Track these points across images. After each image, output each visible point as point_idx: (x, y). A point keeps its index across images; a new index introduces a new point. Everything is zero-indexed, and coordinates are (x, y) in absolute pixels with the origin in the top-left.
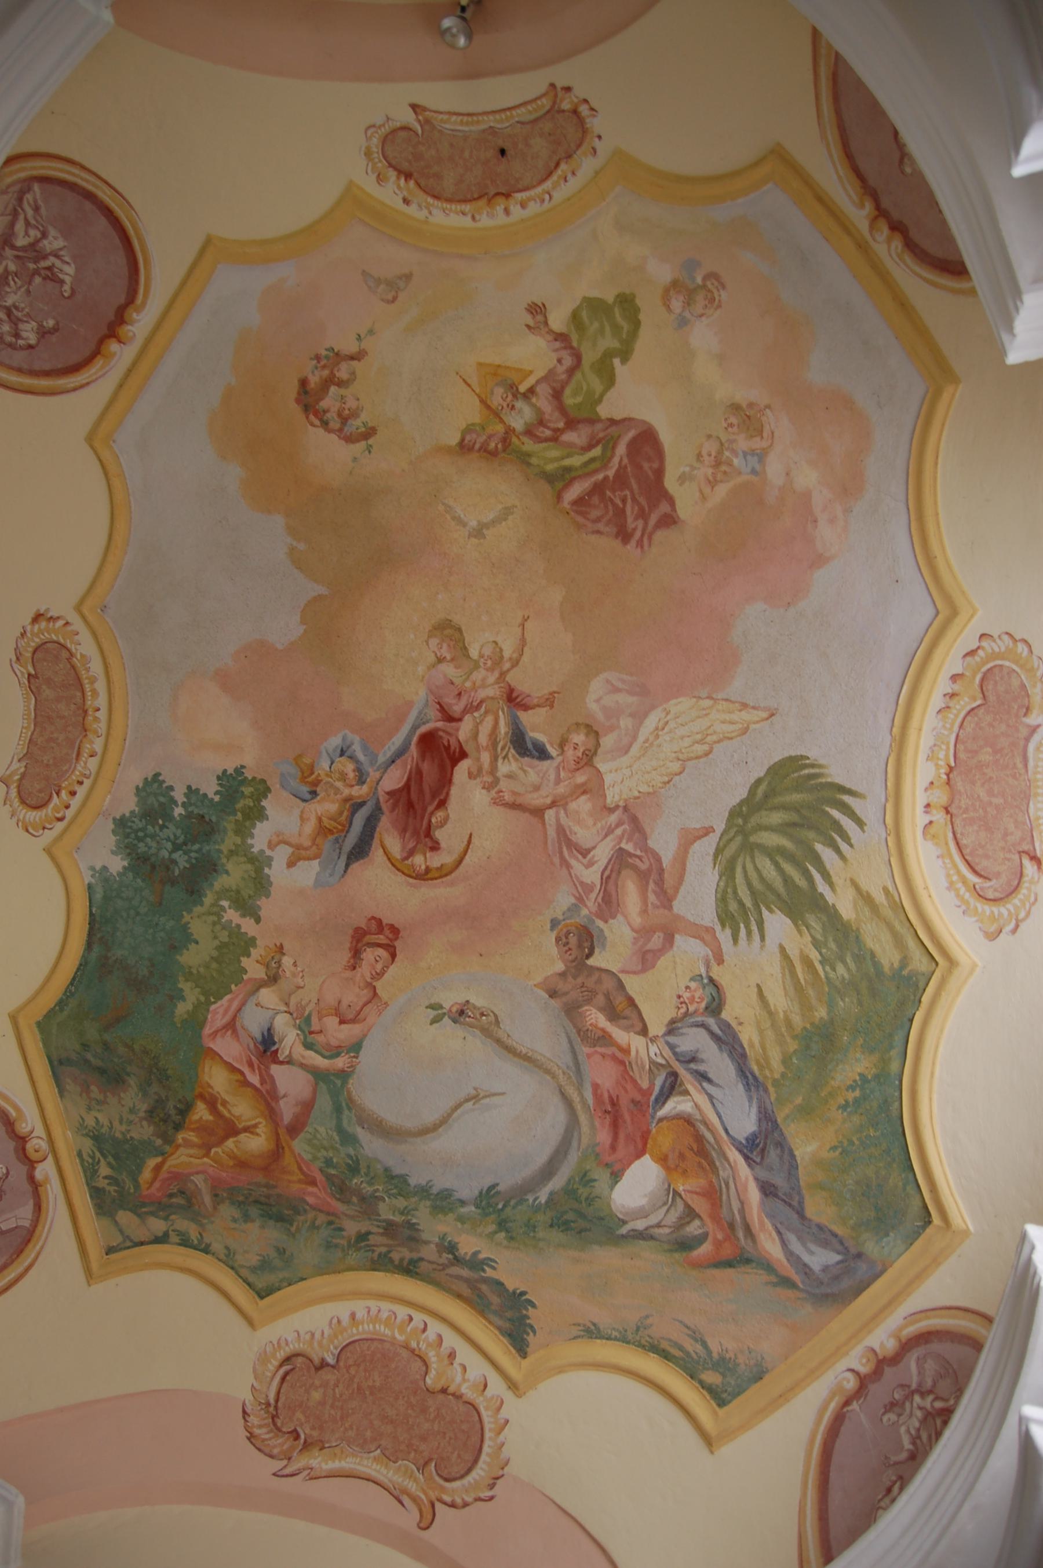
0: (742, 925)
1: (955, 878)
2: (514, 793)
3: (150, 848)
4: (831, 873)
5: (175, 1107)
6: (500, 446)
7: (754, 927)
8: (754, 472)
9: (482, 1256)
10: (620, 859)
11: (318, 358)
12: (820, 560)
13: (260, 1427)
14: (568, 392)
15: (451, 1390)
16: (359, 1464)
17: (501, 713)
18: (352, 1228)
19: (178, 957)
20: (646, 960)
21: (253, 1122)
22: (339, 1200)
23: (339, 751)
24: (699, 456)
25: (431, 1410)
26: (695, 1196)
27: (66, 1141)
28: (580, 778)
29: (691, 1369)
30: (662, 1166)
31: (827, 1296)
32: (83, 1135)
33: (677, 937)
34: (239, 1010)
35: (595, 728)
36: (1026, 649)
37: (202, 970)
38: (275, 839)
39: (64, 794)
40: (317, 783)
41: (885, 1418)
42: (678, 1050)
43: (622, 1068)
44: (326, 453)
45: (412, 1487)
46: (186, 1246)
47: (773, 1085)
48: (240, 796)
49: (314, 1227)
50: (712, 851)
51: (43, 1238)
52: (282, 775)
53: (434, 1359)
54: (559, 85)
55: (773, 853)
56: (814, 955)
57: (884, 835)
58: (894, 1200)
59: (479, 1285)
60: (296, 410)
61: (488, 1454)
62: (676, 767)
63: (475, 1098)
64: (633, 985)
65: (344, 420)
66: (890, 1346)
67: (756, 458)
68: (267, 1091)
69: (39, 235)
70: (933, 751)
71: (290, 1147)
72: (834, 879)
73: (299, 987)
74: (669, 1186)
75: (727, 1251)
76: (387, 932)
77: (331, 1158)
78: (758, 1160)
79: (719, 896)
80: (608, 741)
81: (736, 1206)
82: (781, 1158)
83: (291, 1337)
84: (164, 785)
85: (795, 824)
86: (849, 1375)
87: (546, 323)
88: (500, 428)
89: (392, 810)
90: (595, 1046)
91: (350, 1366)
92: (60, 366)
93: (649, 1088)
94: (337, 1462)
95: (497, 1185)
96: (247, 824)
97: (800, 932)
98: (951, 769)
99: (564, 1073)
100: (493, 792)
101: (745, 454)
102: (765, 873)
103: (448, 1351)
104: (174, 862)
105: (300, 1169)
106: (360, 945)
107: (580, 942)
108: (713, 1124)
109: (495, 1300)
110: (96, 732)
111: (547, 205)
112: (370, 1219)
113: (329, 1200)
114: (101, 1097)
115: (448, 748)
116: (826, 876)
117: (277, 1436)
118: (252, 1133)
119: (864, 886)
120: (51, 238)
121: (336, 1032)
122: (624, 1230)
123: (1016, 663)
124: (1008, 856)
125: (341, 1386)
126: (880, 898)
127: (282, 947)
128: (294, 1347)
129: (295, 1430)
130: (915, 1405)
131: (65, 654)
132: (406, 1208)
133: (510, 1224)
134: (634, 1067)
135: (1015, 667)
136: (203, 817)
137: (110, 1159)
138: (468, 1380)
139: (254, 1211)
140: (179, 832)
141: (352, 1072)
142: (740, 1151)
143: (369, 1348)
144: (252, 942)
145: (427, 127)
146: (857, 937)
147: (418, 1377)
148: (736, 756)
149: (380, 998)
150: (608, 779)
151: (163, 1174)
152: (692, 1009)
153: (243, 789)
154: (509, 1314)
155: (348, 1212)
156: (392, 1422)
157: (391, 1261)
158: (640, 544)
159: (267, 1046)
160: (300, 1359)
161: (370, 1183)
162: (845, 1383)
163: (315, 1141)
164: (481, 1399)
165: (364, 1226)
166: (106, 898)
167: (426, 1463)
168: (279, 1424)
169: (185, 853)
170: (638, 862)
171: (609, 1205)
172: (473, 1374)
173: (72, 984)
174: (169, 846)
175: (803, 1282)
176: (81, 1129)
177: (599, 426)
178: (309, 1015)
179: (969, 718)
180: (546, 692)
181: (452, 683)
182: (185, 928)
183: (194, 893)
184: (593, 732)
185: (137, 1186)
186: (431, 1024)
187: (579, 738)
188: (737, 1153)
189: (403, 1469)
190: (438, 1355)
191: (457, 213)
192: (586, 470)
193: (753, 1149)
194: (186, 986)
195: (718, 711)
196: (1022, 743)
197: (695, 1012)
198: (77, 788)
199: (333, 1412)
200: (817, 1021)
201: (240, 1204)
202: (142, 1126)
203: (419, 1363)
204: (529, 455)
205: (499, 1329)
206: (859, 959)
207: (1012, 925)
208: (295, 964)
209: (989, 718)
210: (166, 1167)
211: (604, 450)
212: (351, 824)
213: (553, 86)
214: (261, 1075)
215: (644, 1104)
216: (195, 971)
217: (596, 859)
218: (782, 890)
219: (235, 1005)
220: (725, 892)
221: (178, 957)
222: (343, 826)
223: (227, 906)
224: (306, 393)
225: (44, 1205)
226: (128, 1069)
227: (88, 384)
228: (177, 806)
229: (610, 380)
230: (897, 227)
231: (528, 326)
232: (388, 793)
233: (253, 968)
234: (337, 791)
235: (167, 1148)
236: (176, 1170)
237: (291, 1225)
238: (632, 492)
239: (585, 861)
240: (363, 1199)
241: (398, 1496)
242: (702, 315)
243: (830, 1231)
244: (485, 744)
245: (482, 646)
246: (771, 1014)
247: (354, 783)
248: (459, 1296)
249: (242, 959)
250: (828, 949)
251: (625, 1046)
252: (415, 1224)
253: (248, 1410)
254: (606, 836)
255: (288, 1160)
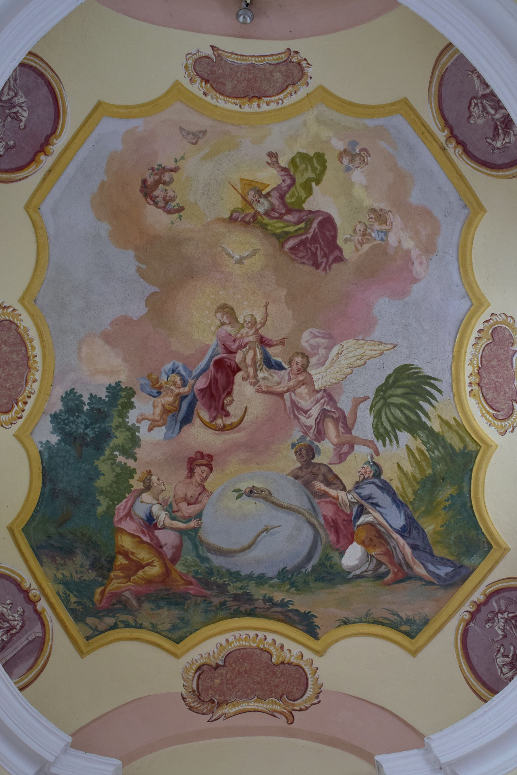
0: (387, 438)
1: (484, 412)
2: (267, 386)
3: (72, 428)
4: (429, 413)
5: (106, 560)
6: (251, 219)
7: (393, 438)
8: (382, 240)
9: (286, 600)
10: (324, 414)
11: (153, 169)
12: (415, 280)
13: (193, 702)
14: (287, 196)
15: (286, 662)
16: (248, 706)
17: (257, 349)
18: (216, 601)
19: (95, 484)
20: (341, 457)
21: (151, 560)
22: (206, 589)
23: (171, 371)
24: (355, 231)
25: (278, 673)
26: (381, 556)
27: (50, 588)
28: (301, 378)
29: (394, 626)
30: (362, 545)
31: (450, 585)
32: (58, 583)
33: (355, 446)
34: (132, 506)
35: (306, 354)
36: (512, 320)
37: (108, 489)
38: (140, 418)
39: (20, 404)
40: (161, 387)
41: (487, 626)
42: (362, 495)
43: (336, 506)
44: (156, 218)
45: (278, 708)
46: (129, 628)
47: (410, 504)
48: (120, 397)
49: (196, 604)
50: (369, 407)
51: (50, 640)
52: (141, 385)
53: (274, 651)
54: (292, 50)
55: (399, 406)
56: (424, 448)
57: (452, 396)
58: (473, 541)
59: (287, 613)
60: (140, 195)
61: (311, 684)
62: (349, 371)
63: (266, 530)
64: (336, 469)
65: (167, 202)
66: (482, 598)
67: (383, 234)
68: (155, 544)
69: (14, 95)
70: (471, 361)
71: (174, 569)
72: (430, 415)
73: (163, 491)
74: (368, 553)
75: (400, 576)
76: (206, 458)
77: (198, 570)
78: (408, 536)
79: (374, 426)
80: (313, 360)
81: (400, 556)
82: (418, 533)
83: (198, 657)
84: (77, 395)
85: (409, 394)
86: (466, 613)
87: (277, 162)
88: (252, 211)
89: (203, 398)
90: (321, 498)
91: (232, 664)
92: (14, 167)
93: (350, 514)
94: (236, 707)
95: (286, 567)
96: (124, 411)
97: (416, 439)
98: (480, 368)
99: (308, 513)
100: (256, 386)
101: (378, 231)
102: (396, 415)
103: (280, 645)
104: (87, 434)
105: (182, 578)
106: (192, 466)
107: (306, 453)
108: (384, 525)
109: (297, 618)
110: (35, 369)
111: (280, 106)
112: (225, 595)
113: (202, 590)
114: (63, 562)
115: (230, 367)
116: (426, 415)
117: (203, 704)
118: (152, 566)
119: (444, 417)
120: (19, 97)
121: (187, 510)
122: (351, 576)
123: (508, 326)
124: (507, 402)
125: (229, 674)
126: (452, 422)
127: (150, 471)
128: (201, 661)
129: (211, 699)
130: (499, 618)
131: (13, 327)
132: (242, 586)
133: (296, 584)
134: (342, 505)
135: (507, 327)
136: (100, 409)
137: (75, 593)
138: (293, 656)
139: (162, 603)
140: (87, 419)
141: (200, 528)
142: (399, 534)
143: (239, 653)
144: (134, 471)
145: (219, 58)
146: (443, 439)
147: (268, 660)
148: (378, 365)
149: (208, 491)
150: (315, 378)
151: (107, 594)
152: (366, 476)
153: (121, 393)
154: (305, 623)
155: (212, 594)
156: (259, 683)
157: (241, 612)
158: (325, 269)
159: (150, 522)
160: (205, 667)
161: (221, 579)
162: (465, 617)
163: (187, 564)
164: (302, 662)
165: (222, 599)
166: (50, 457)
167: (281, 697)
168: (202, 699)
169: (92, 429)
170: (333, 414)
171: (341, 567)
172: (295, 652)
173: (37, 506)
174: (83, 426)
175: (437, 582)
176: (56, 580)
177: (303, 214)
178: (171, 504)
179: (487, 347)
180: (280, 338)
181: (230, 335)
182: (96, 467)
183: (99, 449)
184: (305, 356)
185: (93, 603)
186: (237, 499)
187: (299, 359)
188: (397, 535)
189: (271, 702)
190: (275, 648)
191: (232, 103)
192: (297, 234)
193: (404, 532)
194: (101, 498)
195: (368, 345)
196: (510, 357)
197: (368, 477)
198: (27, 400)
199: (228, 686)
200: (428, 475)
201: (153, 601)
202: (89, 573)
203: (267, 654)
204: (267, 225)
205: (301, 630)
206: (445, 448)
207: (511, 429)
208: (159, 479)
209: (495, 347)
210: (107, 591)
211: (306, 224)
212: (180, 407)
213: (289, 49)
214: (150, 537)
215: (351, 520)
216: (105, 490)
217: (312, 414)
218: (405, 422)
219: (129, 504)
220: (377, 424)
221: (95, 484)
222: (176, 408)
223: (118, 455)
224: (146, 187)
225: (46, 624)
226: (75, 545)
227: (27, 177)
228: (85, 405)
229: (309, 192)
230: (459, 143)
231: (267, 162)
232: (199, 390)
233: (136, 484)
234: (172, 391)
235: (105, 581)
236: (113, 591)
237: (184, 606)
238: (320, 245)
239: (307, 416)
240: (219, 586)
241: (272, 714)
242: (358, 167)
243: (447, 559)
244: (250, 364)
245: (245, 317)
246: (405, 474)
247: (181, 386)
248: (279, 620)
249: (129, 480)
250: (430, 445)
251: (336, 497)
252: (249, 593)
253: (185, 696)
254: (316, 403)
255: (174, 575)
